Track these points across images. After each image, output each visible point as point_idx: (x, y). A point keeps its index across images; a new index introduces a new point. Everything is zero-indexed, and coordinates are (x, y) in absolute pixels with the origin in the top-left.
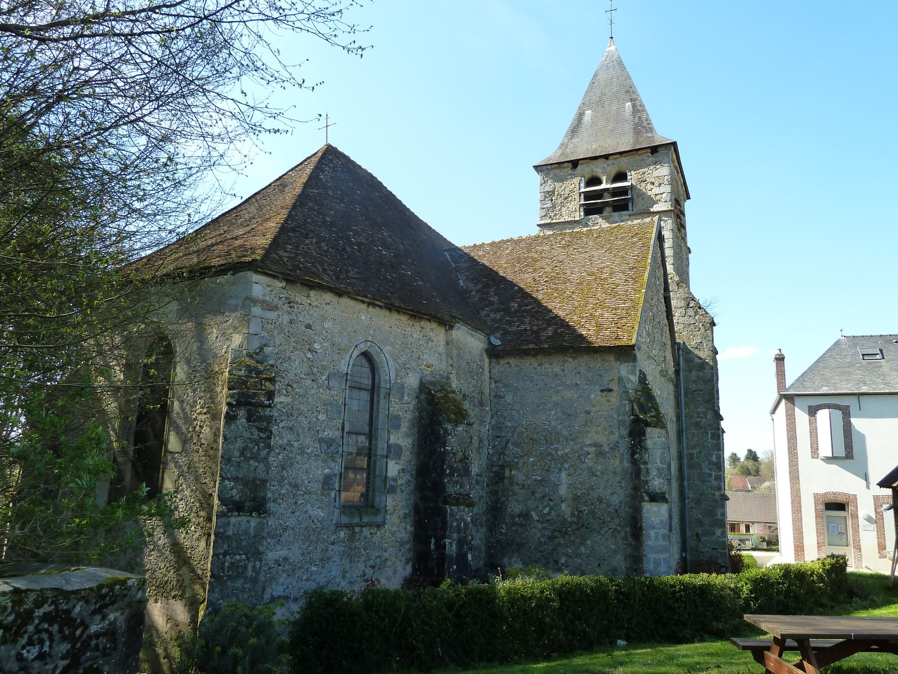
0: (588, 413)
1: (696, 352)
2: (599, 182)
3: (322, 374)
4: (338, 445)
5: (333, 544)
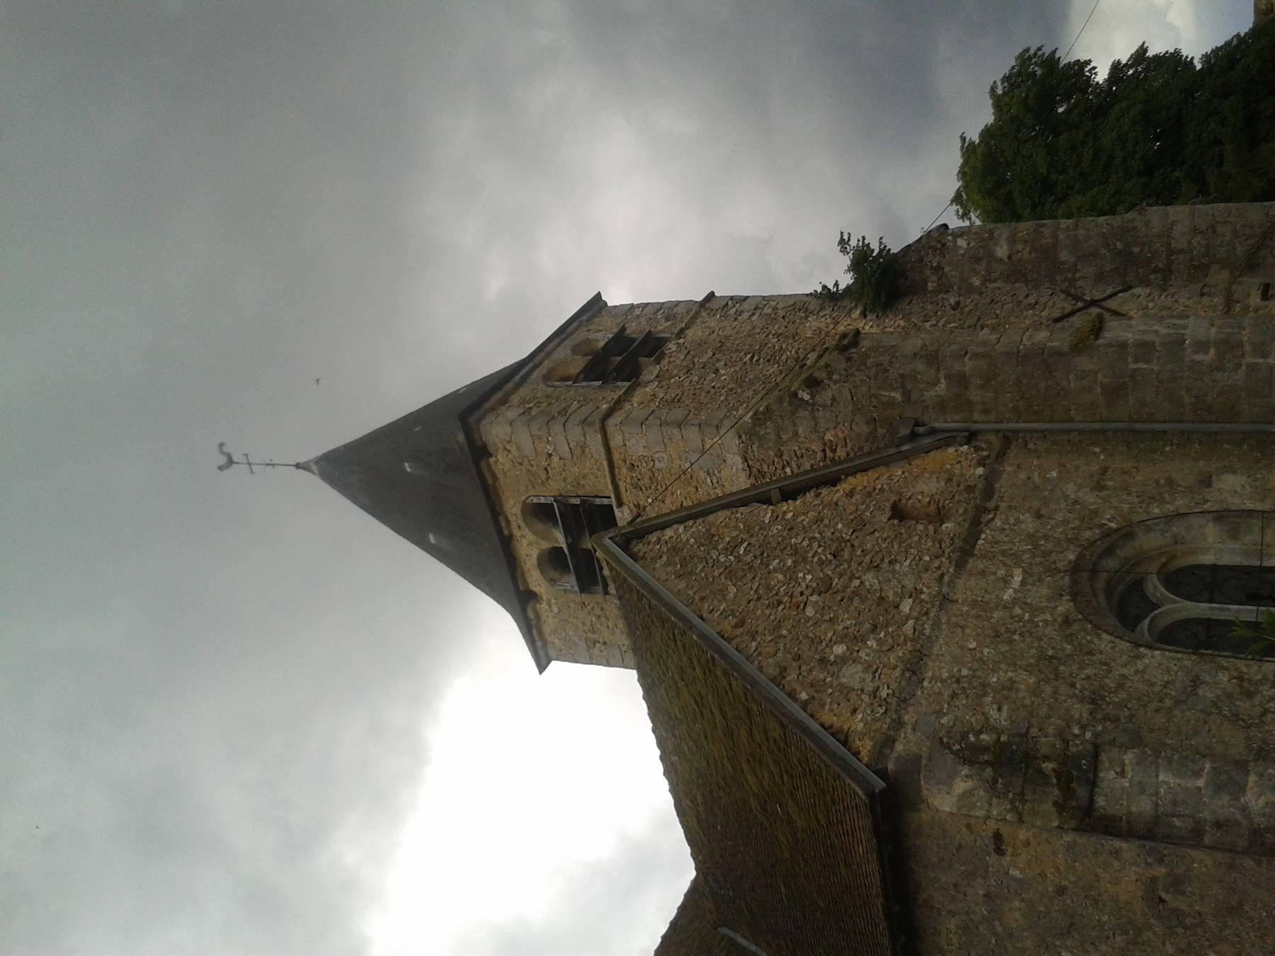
0: (1061, 891)
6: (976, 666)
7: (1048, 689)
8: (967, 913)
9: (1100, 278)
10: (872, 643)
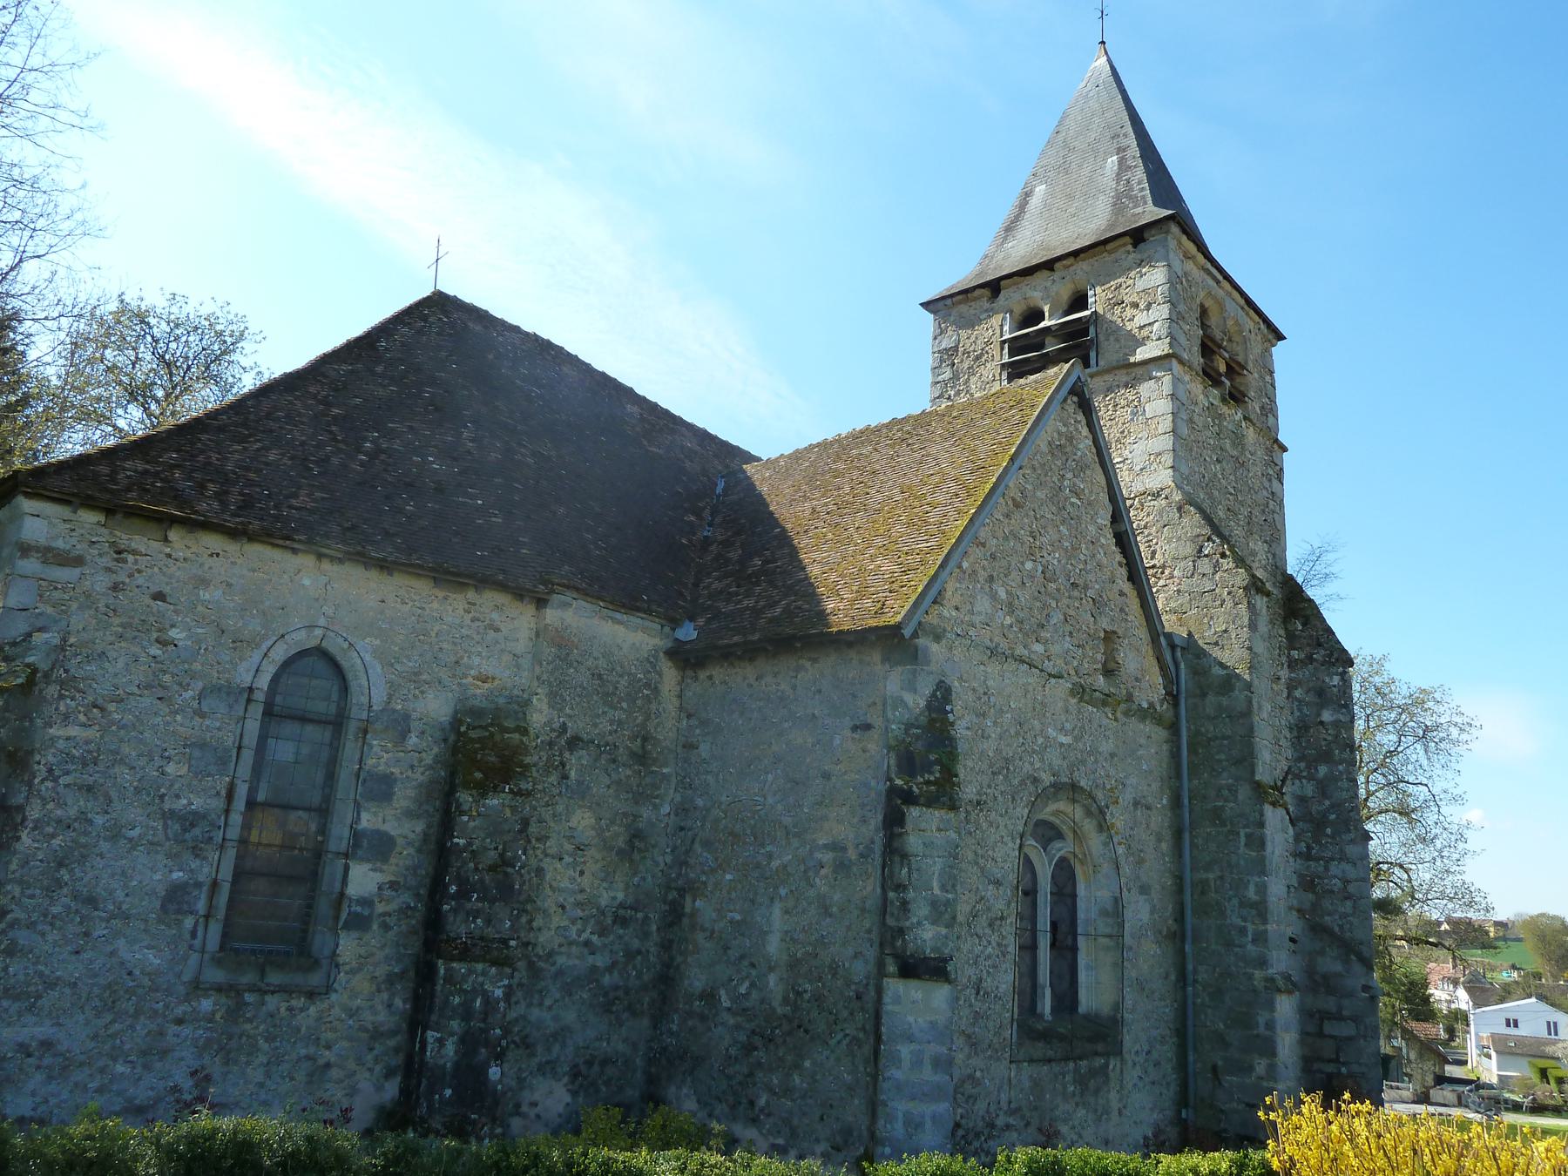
0: (827, 776)
1: (1216, 653)
2: (1040, 316)
3: (186, 687)
4: (212, 824)
5: (180, 1022)
6: (998, 707)
7: (985, 766)
8: (796, 700)
9: (1302, 800)
10: (1008, 620)
